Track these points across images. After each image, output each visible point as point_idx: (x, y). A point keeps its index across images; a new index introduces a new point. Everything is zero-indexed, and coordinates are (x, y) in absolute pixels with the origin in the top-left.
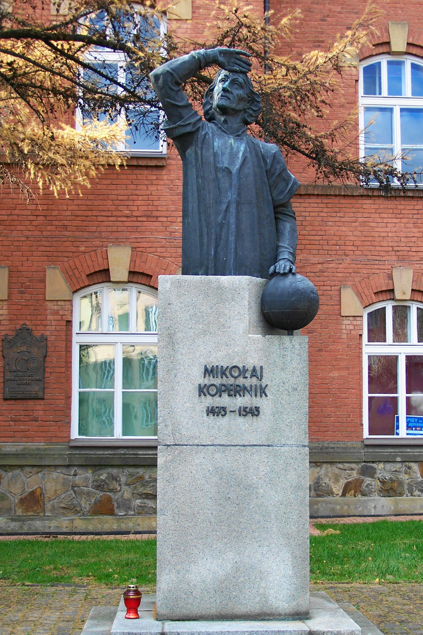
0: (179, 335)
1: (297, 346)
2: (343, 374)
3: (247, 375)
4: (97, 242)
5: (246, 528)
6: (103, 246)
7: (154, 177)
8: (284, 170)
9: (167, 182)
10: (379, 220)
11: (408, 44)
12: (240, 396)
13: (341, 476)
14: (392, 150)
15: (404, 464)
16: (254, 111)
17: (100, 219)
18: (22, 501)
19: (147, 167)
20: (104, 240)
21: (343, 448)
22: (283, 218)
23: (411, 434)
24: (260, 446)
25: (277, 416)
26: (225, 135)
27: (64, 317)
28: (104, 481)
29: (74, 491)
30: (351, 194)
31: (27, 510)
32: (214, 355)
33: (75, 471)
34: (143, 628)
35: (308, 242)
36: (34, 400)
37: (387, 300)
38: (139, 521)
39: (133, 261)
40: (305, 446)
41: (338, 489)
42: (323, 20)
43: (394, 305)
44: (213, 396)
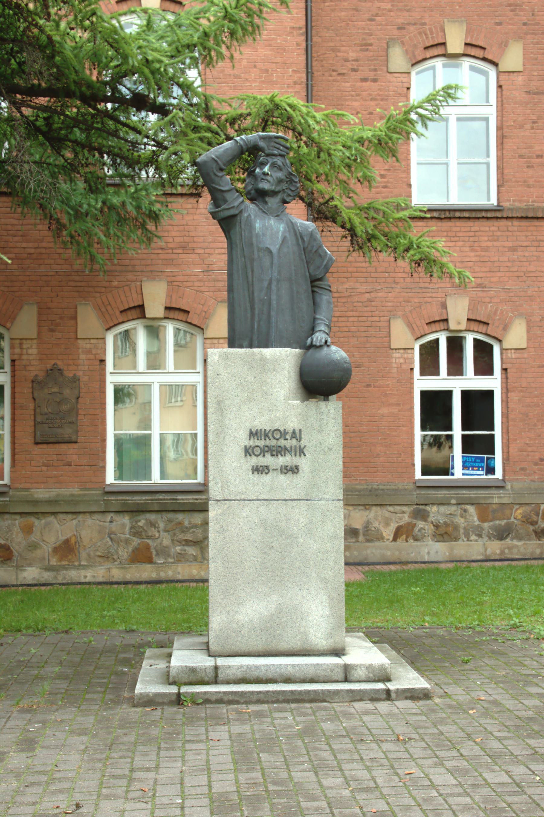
0: (227, 402)
1: (332, 411)
2: (393, 411)
3: (287, 437)
6: (136, 281)
8: (320, 247)
11: (466, 44)
12: (282, 455)
13: (391, 519)
15: (459, 506)
18: (56, 550)
21: (393, 490)
23: (467, 475)
24: (300, 500)
25: (314, 473)
26: (266, 216)
27: (97, 356)
28: (142, 527)
29: (111, 539)
31: (61, 560)
32: (258, 420)
33: (112, 517)
34: (198, 662)
35: (355, 269)
36: (67, 444)
37: (441, 330)
38: (180, 569)
39: (169, 296)
40: (339, 500)
41: (388, 533)
42: (371, 20)
43: (448, 335)
44: (257, 456)
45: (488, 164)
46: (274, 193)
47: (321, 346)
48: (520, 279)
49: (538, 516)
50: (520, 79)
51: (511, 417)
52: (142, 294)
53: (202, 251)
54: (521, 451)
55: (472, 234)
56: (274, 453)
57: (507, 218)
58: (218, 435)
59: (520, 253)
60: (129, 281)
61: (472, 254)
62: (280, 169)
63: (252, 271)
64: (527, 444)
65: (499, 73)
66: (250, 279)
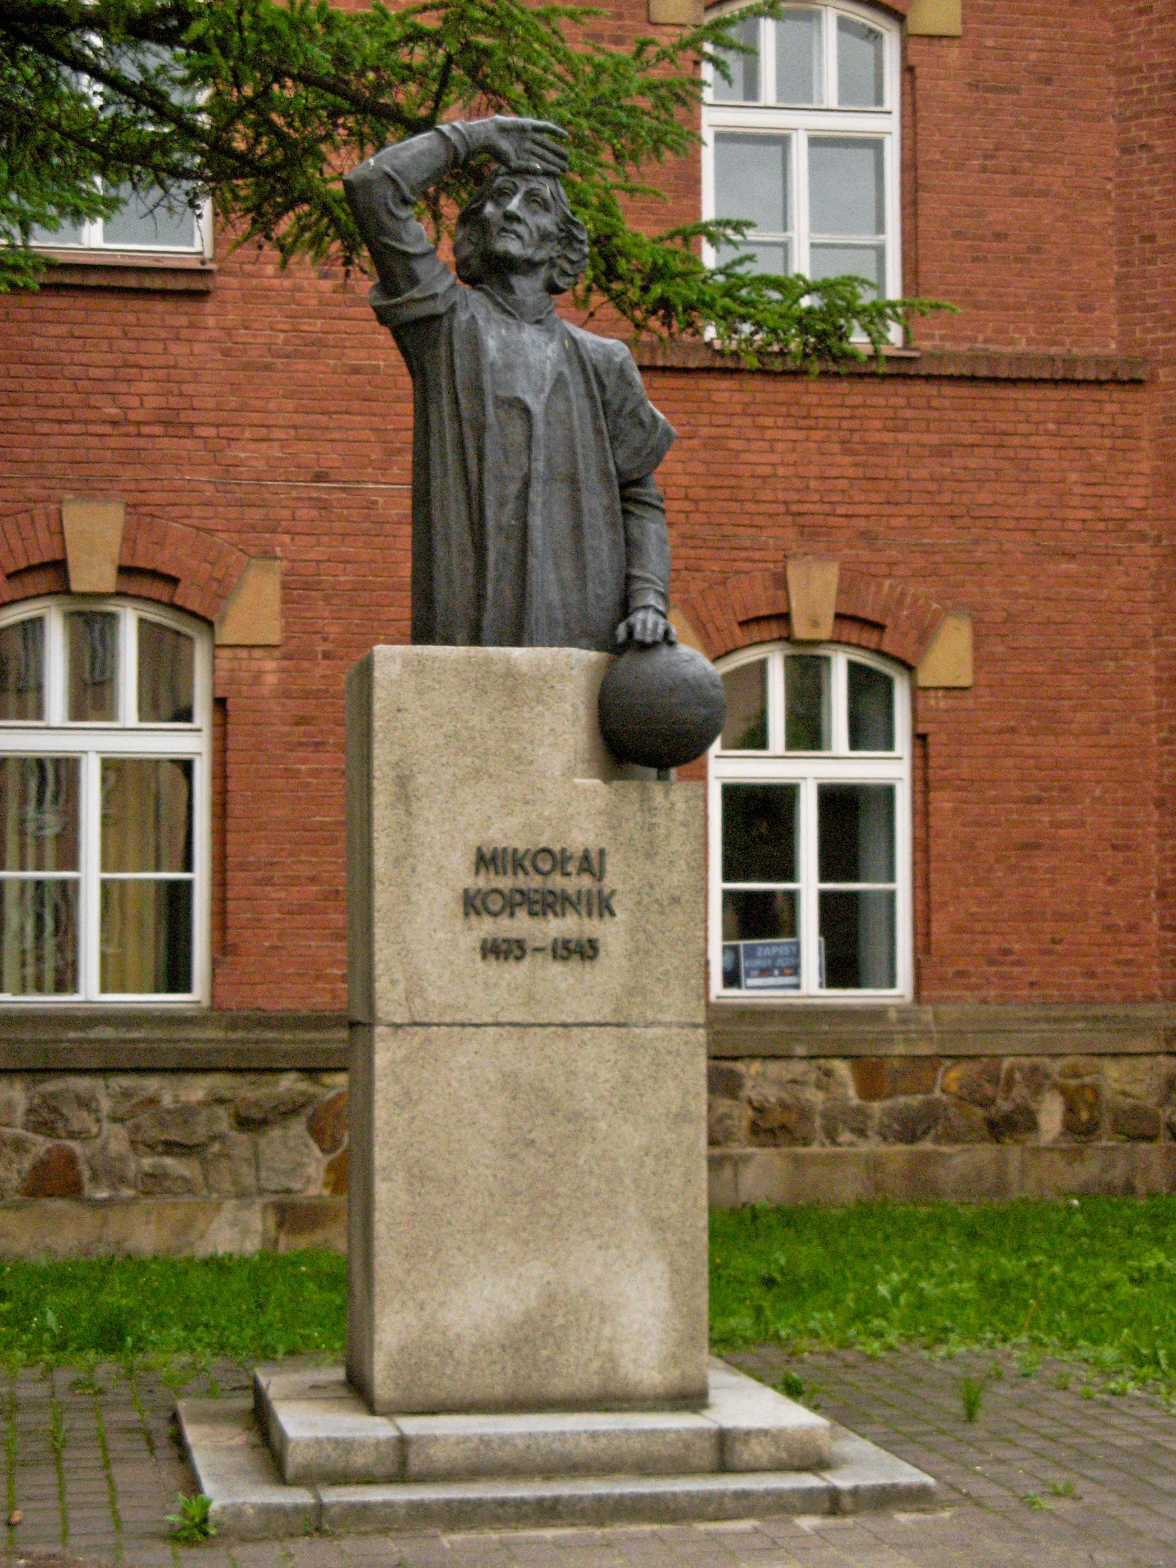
0: (422, 779)
1: (680, 806)
4: (33, 489)
5: (569, 1208)
6: (48, 499)
7: (183, 320)
9: (216, 333)
10: (754, 434)
14: (785, 246)
15: (814, 1063)
16: (572, 262)
17: (46, 428)
19: (164, 294)
20: (53, 483)
22: (637, 512)
25: (636, 959)
26: (511, 321)
30: (681, 365)
39: (129, 539)
40: (696, 1026)
44: (496, 915)
45: (880, 251)
46: (531, 266)
47: (654, 645)
48: (959, 522)
49: (997, 1083)
50: (953, 54)
51: (935, 850)
52: (62, 533)
53: (211, 432)
54: (960, 930)
55: (846, 412)
56: (537, 908)
57: (928, 378)
58: (398, 861)
59: (957, 461)
60: (30, 500)
61: (848, 459)
62: (546, 208)
63: (481, 457)
64: (972, 915)
65: (907, 40)
66: (474, 477)
